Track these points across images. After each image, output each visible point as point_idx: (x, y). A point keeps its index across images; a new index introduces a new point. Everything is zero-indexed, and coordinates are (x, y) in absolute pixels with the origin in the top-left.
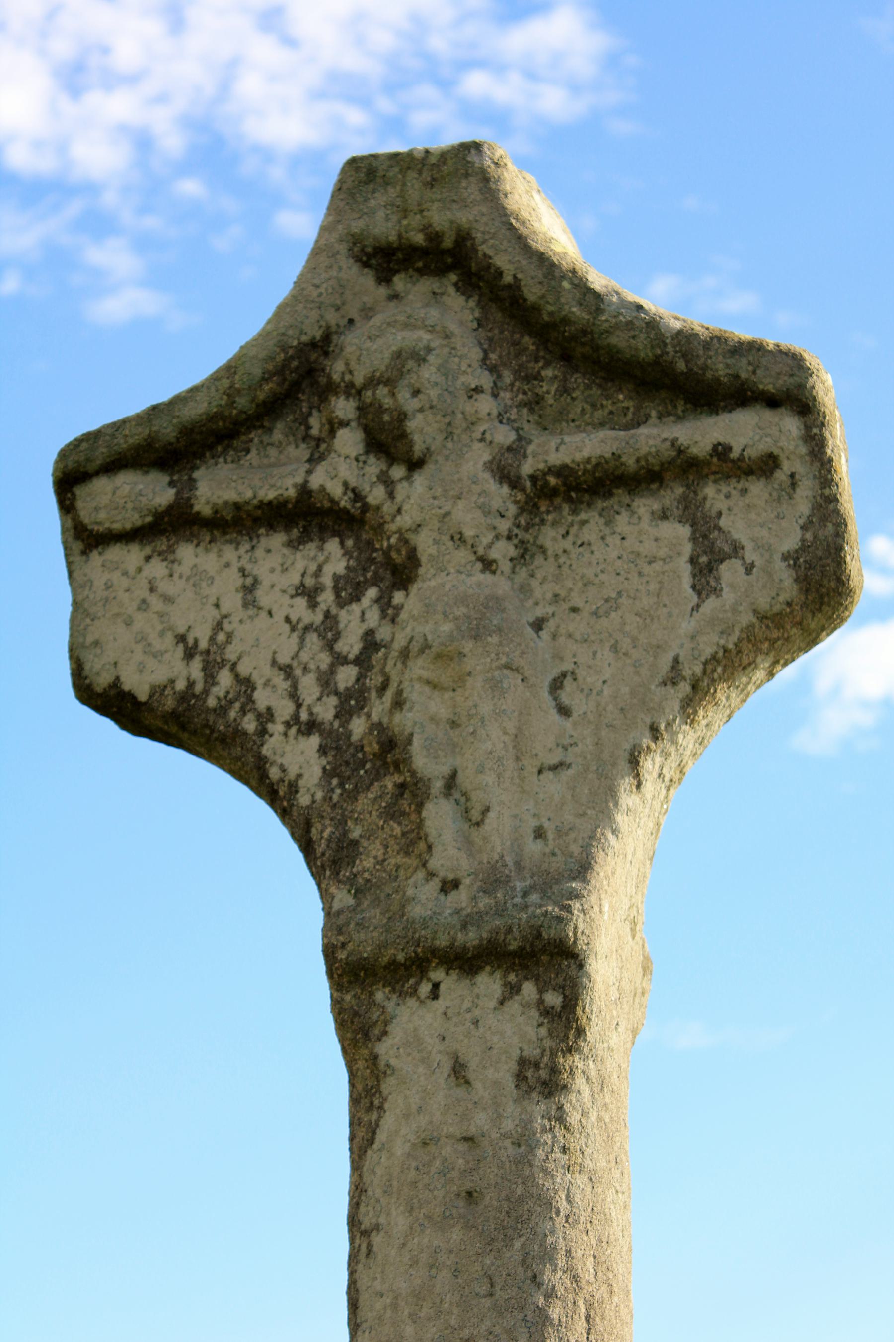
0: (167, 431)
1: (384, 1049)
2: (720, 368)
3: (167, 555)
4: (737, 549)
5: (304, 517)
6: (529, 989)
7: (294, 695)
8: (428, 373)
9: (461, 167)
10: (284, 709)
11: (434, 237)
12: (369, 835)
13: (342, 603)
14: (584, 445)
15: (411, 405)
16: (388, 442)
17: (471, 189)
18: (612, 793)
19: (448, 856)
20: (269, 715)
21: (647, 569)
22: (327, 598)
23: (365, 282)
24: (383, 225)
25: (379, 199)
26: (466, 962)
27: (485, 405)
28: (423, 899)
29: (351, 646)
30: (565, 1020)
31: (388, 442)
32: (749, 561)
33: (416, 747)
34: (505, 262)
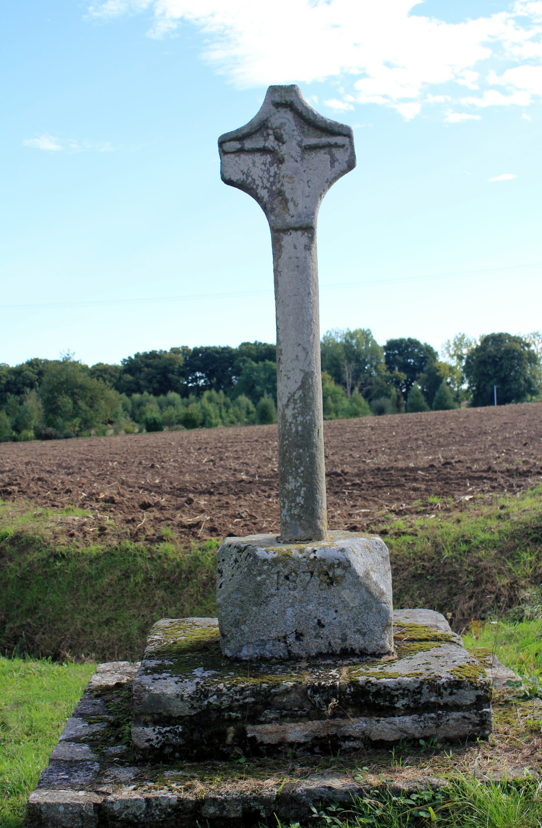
0: (240, 135)
1: (282, 243)
2: (336, 129)
3: (239, 156)
4: (338, 160)
5: (264, 151)
6: (306, 234)
7: (262, 182)
8: (286, 127)
9: (292, 89)
10: (261, 184)
11: (287, 102)
12: (277, 207)
13: (270, 166)
14: (313, 141)
15: (283, 132)
16: (279, 139)
17: (293, 94)
18: (317, 201)
19: (292, 211)
20: (258, 185)
22: (268, 165)
23: (273, 109)
24: (278, 99)
25: (277, 94)
26: (296, 229)
27: (296, 133)
28: (289, 219)
30: (312, 239)
31: (279, 139)
33: (286, 193)
34: (300, 108)
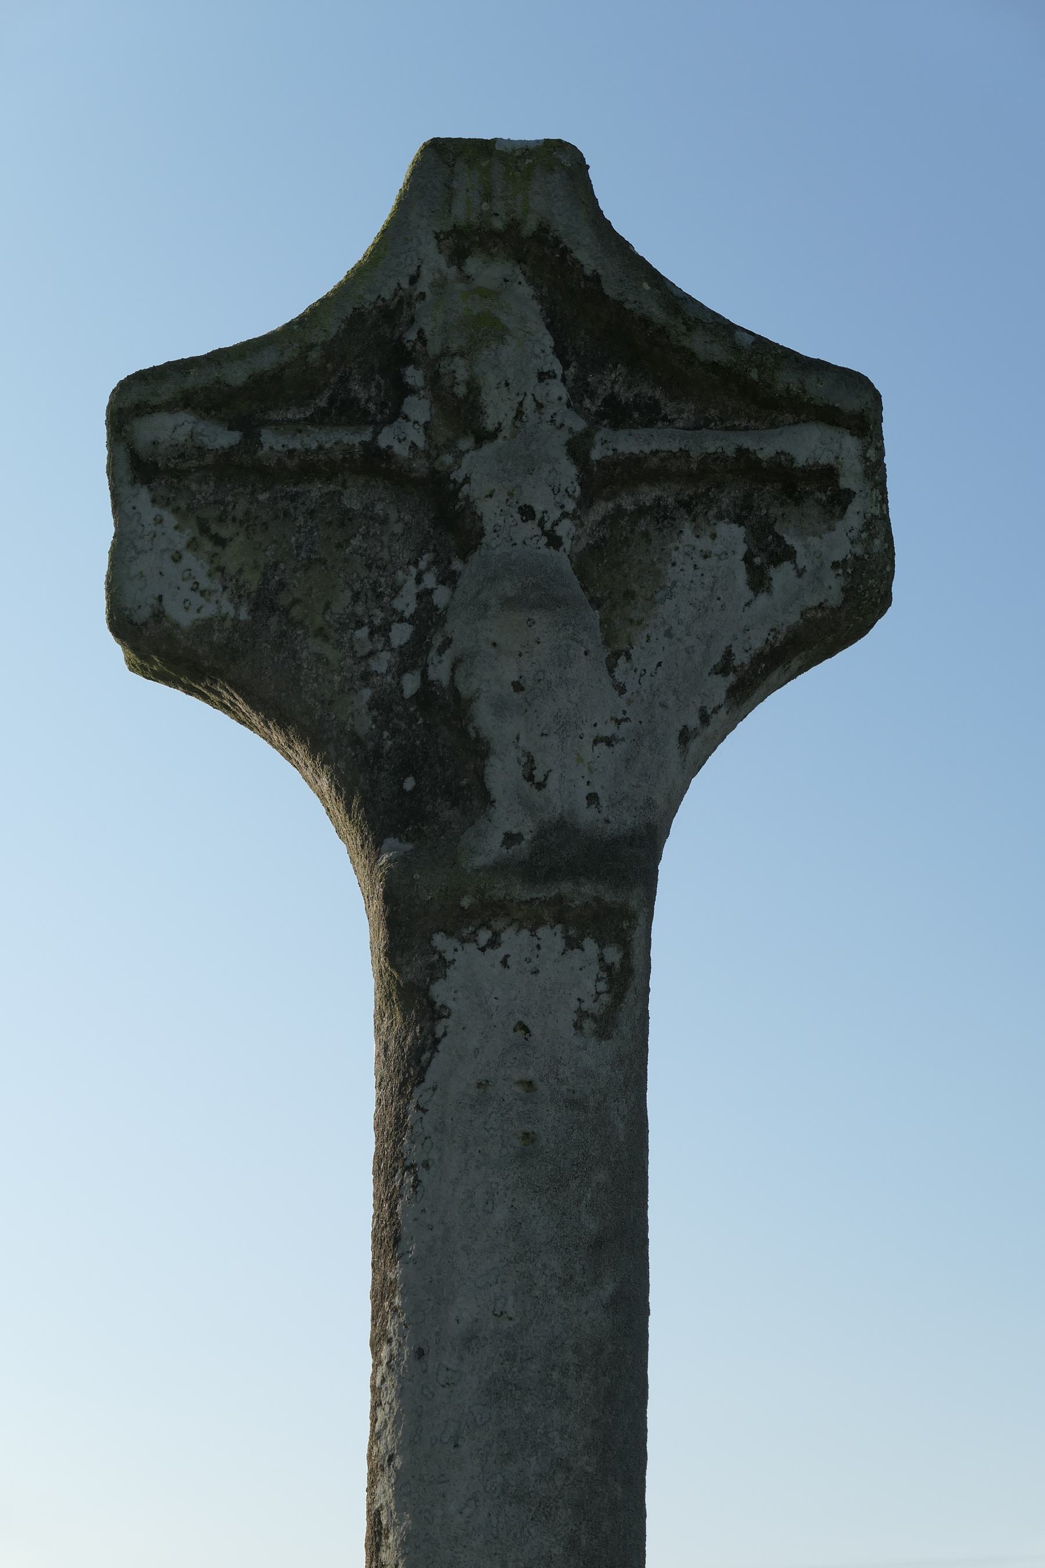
6: (590, 946)
21: (701, 563)
29: (408, 605)
32: (800, 567)
